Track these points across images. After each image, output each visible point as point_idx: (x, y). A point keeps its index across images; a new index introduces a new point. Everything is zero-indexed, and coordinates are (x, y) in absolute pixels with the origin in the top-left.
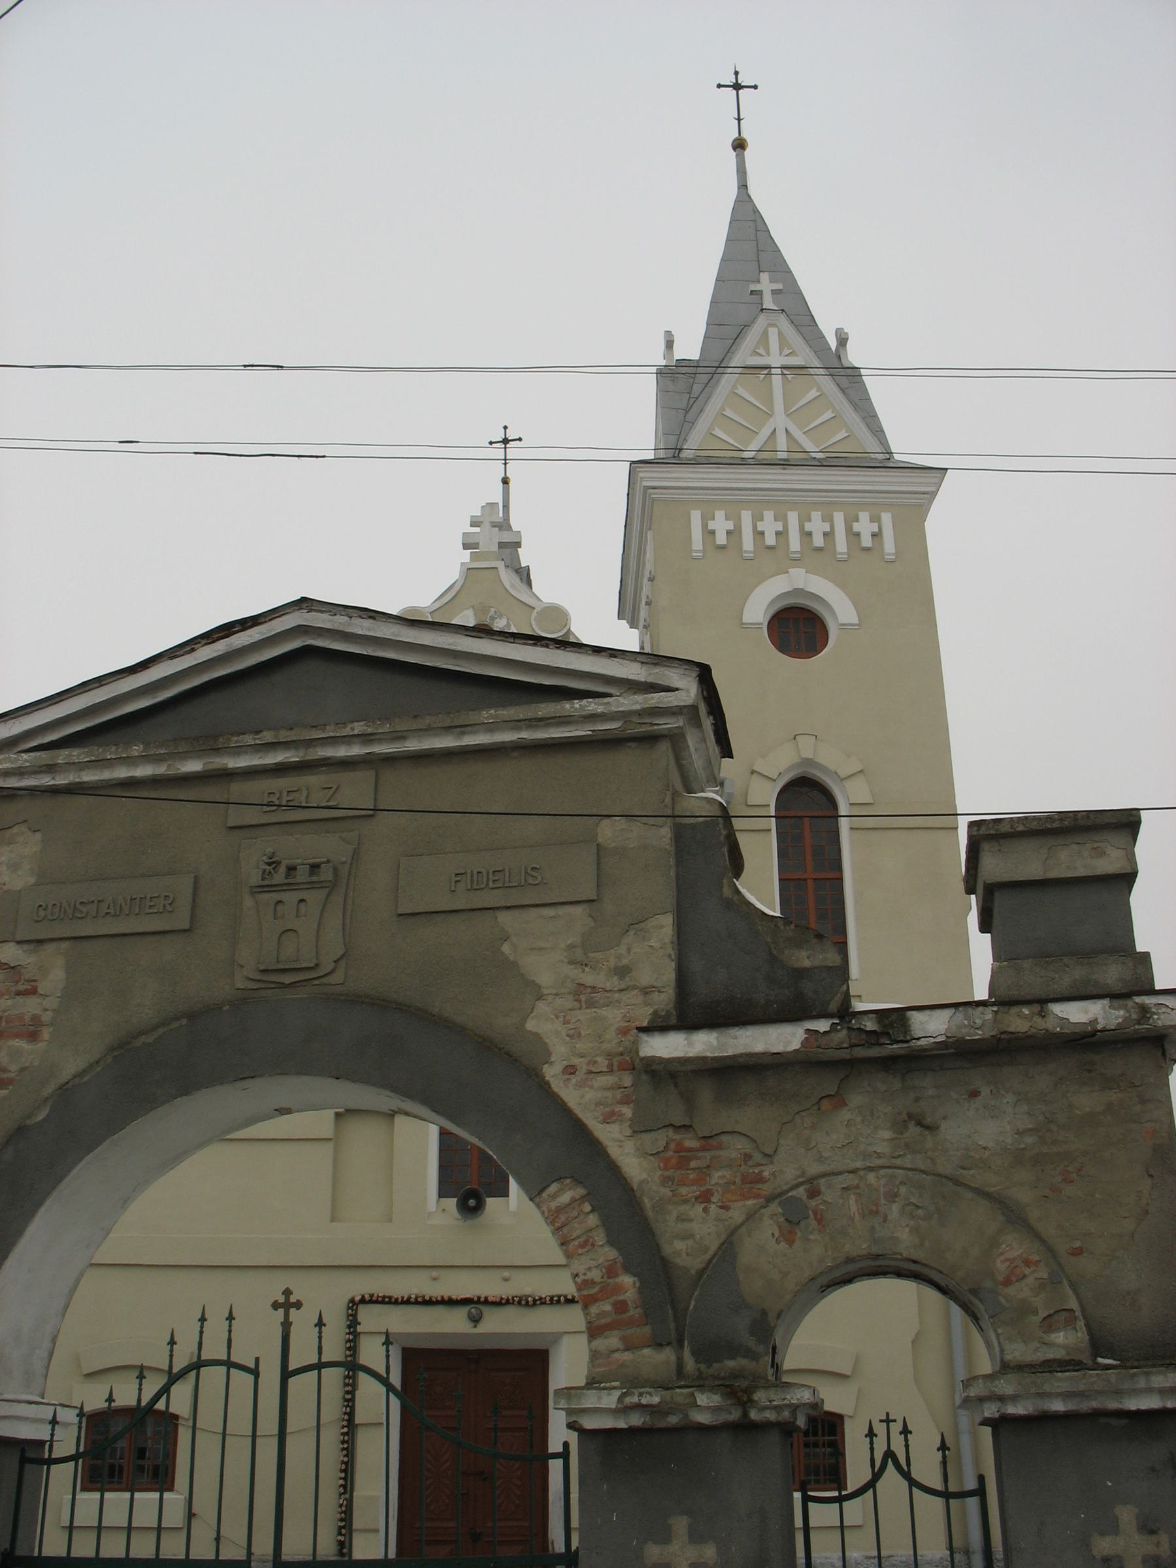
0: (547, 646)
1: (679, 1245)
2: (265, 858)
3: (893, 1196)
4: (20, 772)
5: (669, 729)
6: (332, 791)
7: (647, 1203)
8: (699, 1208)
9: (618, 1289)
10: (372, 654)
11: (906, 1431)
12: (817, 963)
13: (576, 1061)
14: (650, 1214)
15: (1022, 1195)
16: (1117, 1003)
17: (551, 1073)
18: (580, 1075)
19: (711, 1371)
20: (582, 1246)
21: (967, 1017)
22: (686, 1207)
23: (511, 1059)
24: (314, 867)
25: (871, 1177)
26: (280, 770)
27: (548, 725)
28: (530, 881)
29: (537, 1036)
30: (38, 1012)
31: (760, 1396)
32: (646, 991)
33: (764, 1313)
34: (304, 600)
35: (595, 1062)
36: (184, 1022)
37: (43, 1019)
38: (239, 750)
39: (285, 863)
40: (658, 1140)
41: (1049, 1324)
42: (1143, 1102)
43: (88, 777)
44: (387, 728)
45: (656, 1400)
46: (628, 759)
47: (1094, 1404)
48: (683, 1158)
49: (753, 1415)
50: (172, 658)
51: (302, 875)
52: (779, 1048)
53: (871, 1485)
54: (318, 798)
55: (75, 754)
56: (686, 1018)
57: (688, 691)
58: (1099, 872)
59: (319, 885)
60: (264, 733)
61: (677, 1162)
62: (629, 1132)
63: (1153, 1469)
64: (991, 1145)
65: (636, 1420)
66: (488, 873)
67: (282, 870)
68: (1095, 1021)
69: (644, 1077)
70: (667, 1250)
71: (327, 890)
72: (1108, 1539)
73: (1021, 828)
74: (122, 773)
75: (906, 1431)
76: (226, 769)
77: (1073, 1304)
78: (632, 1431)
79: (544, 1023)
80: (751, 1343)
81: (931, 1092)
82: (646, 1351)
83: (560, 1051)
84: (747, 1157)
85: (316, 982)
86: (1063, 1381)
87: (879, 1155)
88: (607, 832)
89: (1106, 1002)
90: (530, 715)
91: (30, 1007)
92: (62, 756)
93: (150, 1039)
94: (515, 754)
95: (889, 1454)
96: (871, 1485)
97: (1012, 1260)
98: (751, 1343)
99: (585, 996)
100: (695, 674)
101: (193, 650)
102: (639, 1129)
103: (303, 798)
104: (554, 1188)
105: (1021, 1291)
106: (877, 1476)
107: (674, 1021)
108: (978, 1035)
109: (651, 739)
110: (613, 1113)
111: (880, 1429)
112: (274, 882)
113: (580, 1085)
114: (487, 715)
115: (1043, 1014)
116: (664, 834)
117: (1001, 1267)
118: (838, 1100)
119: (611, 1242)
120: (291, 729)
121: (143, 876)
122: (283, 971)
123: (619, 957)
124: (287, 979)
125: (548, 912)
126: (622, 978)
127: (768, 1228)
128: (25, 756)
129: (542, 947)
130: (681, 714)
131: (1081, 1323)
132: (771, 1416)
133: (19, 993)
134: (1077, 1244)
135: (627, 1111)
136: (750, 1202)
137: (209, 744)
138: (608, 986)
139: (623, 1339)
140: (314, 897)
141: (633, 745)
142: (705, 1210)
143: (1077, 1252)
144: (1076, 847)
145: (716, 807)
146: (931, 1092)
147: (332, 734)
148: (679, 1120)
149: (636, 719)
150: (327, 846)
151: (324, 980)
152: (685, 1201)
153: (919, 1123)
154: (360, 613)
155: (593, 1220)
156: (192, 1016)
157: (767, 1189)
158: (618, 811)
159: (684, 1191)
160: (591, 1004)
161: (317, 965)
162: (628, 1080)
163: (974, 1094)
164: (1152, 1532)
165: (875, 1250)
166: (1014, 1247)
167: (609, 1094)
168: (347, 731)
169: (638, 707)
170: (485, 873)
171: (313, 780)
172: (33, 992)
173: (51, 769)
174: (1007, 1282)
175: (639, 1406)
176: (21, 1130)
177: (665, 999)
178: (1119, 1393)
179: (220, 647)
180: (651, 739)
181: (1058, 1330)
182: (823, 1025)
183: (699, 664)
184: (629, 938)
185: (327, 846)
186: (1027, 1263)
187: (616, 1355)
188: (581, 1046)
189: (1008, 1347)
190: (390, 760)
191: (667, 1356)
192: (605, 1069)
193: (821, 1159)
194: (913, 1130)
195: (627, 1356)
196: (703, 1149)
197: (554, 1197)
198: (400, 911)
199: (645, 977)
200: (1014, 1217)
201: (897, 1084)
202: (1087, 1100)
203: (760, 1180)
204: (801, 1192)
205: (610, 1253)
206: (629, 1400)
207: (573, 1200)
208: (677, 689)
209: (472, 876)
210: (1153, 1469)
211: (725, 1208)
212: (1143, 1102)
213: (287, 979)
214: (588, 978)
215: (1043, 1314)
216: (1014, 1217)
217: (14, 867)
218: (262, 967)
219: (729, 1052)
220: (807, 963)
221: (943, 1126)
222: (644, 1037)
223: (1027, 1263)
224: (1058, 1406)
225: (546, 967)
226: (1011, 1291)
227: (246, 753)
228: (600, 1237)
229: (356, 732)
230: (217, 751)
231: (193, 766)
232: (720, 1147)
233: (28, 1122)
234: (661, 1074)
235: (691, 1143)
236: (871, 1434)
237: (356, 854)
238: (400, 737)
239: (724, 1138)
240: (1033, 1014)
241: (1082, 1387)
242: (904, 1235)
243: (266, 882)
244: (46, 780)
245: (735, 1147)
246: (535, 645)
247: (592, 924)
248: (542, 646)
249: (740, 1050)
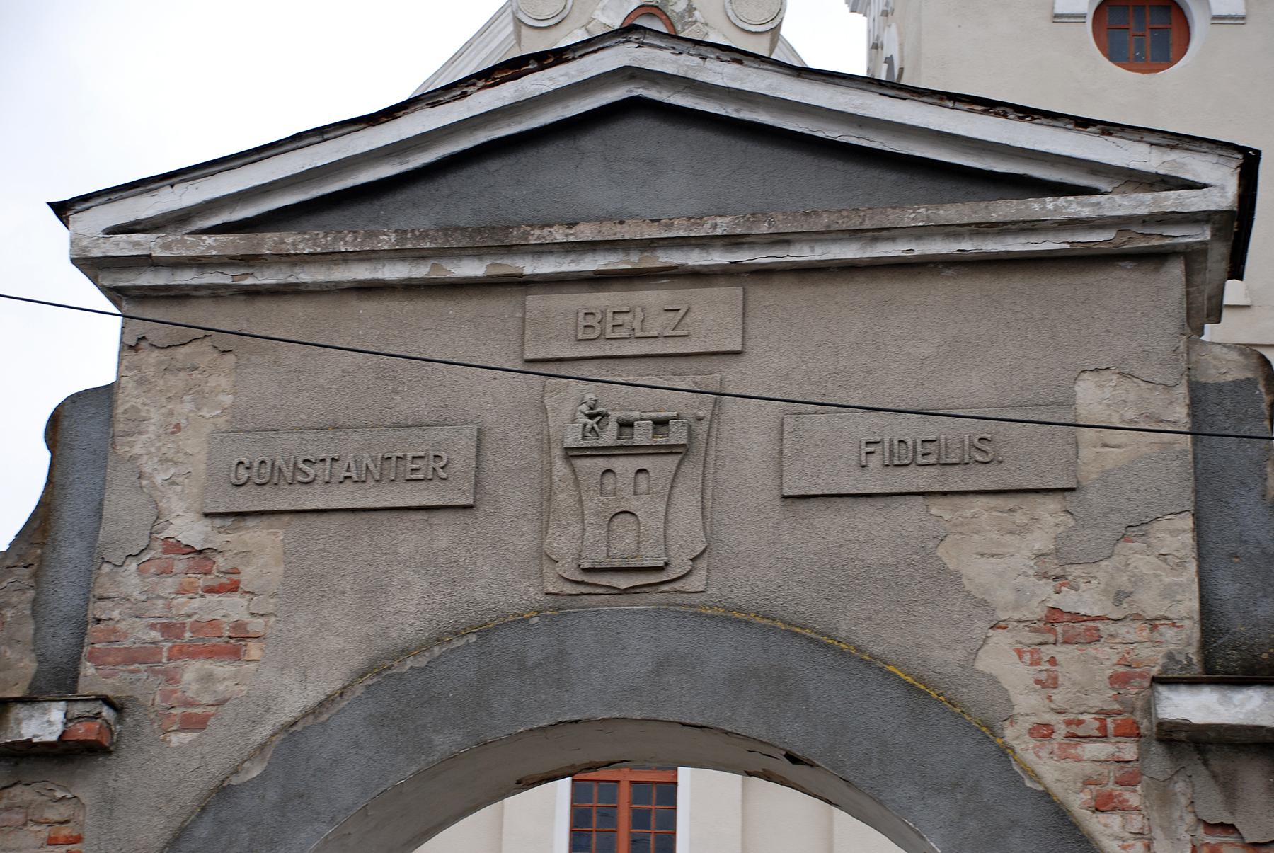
0: (1005, 116)
2: (584, 408)
4: (199, 263)
5: (1187, 245)
6: (682, 313)
10: (734, 115)
24: (661, 423)
28: (979, 458)
30: (245, 618)
35: (1080, 722)
36: (473, 638)
37: (250, 628)
39: (614, 416)
50: (433, 105)
51: (642, 435)
57: (1223, 188)
59: (669, 450)
60: (582, 227)
66: (915, 443)
67: (613, 426)
69: (1156, 749)
71: (679, 457)
76: (520, 276)
79: (1003, 663)
85: (665, 588)
91: (232, 608)
92: (268, 242)
93: (422, 661)
94: (949, 272)
100: (1235, 164)
101: (465, 95)
103: (637, 324)
107: (1197, 671)
109: (1156, 257)
112: (602, 443)
120: (621, 223)
121: (400, 425)
128: (209, 240)
130: (1207, 222)
133: (210, 590)
140: (661, 466)
141: (1129, 265)
147: (682, 233)
151: (677, 586)
154: (719, 53)
156: (484, 631)
161: (666, 564)
162: (1129, 751)
170: (910, 444)
171: (652, 298)
172: (234, 588)
176: (223, 791)
177: (1182, 639)
183: (1243, 150)
188: (1059, 697)
192: (1097, 733)
198: (786, 492)
208: (1205, 186)
209: (891, 445)
213: (623, 582)
214: (1068, 601)
218: (586, 565)
227: (551, 253)
229: (719, 232)
230: (509, 249)
233: (235, 780)
234: (1187, 742)
243: (588, 443)
246: (986, 112)
247: (1072, 523)
248: (997, 114)
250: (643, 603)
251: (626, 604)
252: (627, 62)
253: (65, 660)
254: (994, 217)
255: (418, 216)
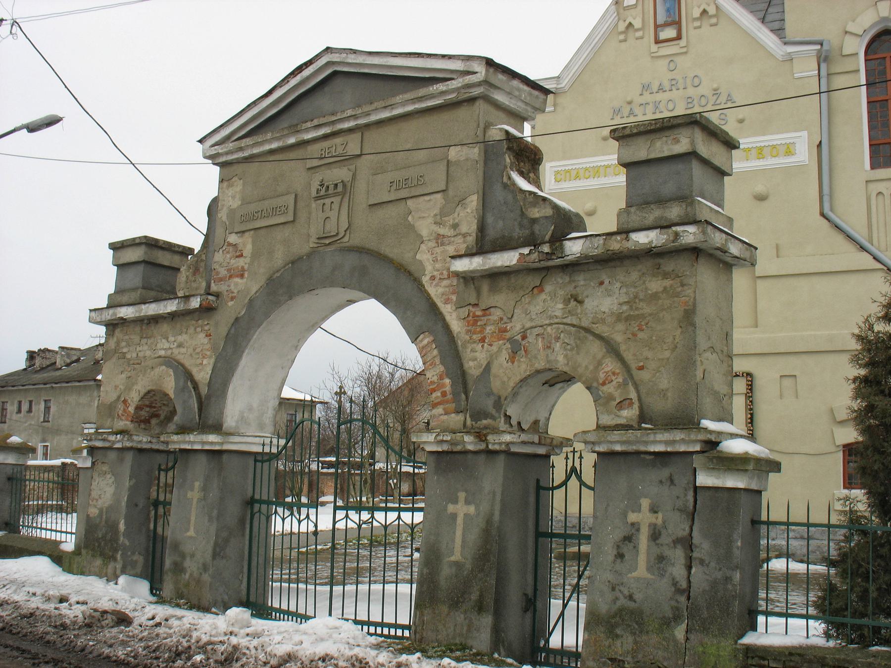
1: (471, 364)
3: (557, 339)
7: (460, 343)
8: (480, 345)
9: (443, 385)
11: (581, 457)
12: (542, 215)
13: (435, 273)
14: (460, 348)
15: (619, 338)
16: (664, 231)
17: (425, 280)
18: (437, 280)
19: (477, 425)
20: (431, 365)
21: (591, 243)
22: (475, 345)
23: (410, 273)
25: (549, 329)
26: (326, 137)
27: (427, 99)
29: (420, 261)
31: (490, 438)
32: (465, 236)
33: (500, 397)
34: (328, 48)
38: (307, 130)
40: (464, 312)
41: (620, 406)
42: (682, 285)
43: (256, 151)
44: (360, 111)
45: (449, 438)
46: (463, 113)
47: (635, 448)
48: (476, 319)
49: (490, 447)
52: (507, 264)
53: (564, 483)
54: (340, 150)
55: (248, 141)
56: (482, 247)
58: (674, 153)
61: (472, 321)
62: (454, 308)
63: (661, 482)
64: (607, 311)
65: (445, 447)
68: (651, 242)
69: (461, 280)
70: (466, 366)
72: (635, 514)
73: (635, 131)
74: (267, 147)
75: (581, 457)
77: (633, 395)
78: (443, 452)
79: (424, 256)
80: (493, 412)
81: (582, 283)
82: (453, 415)
83: (429, 268)
84: (501, 319)
86: (616, 436)
87: (557, 317)
88: (453, 153)
89: (658, 231)
90: (416, 96)
91: (241, 262)
92: (244, 143)
95: (574, 469)
96: (564, 483)
97: (607, 373)
98: (493, 412)
99: (440, 240)
102: (459, 307)
104: (421, 337)
105: (609, 389)
106: (568, 478)
108: (596, 252)
109: (472, 100)
110: (448, 299)
111: (570, 456)
113: (437, 285)
114: (398, 99)
115: (627, 239)
116: (475, 152)
117: (602, 376)
118: (540, 288)
119: (442, 363)
122: (326, 237)
123: (454, 219)
124: (327, 241)
125: (427, 198)
126: (455, 230)
127: (505, 355)
129: (424, 217)
131: (636, 406)
132: (497, 447)
134: (641, 364)
135: (454, 298)
136: (501, 342)
137: (295, 129)
138: (449, 234)
139: (444, 409)
142: (483, 346)
143: (641, 368)
144: (664, 139)
145: (503, 133)
146: (582, 283)
148: (473, 301)
149: (463, 91)
150: (341, 174)
152: (475, 342)
153: (576, 300)
155: (435, 352)
157: (508, 335)
158: (457, 142)
159: (474, 337)
160: (443, 244)
163: (602, 283)
164: (656, 512)
165: (547, 366)
166: (610, 365)
167: (447, 289)
168: (345, 115)
169: (460, 85)
171: (338, 140)
173: (241, 149)
174: (604, 384)
175: (442, 441)
176: (237, 319)
178: (646, 443)
179: (298, 78)
180: (472, 100)
181: (624, 409)
182: (526, 251)
184: (458, 209)
185: (341, 174)
186: (614, 374)
187: (442, 417)
188: (438, 266)
189: (600, 417)
190: (367, 126)
191: (460, 417)
193: (531, 320)
194: (573, 303)
195: (446, 417)
196: (484, 315)
197: (421, 341)
199: (464, 229)
200: (613, 350)
201: (567, 279)
202: (655, 285)
203: (505, 331)
204: (519, 337)
205: (441, 368)
206: (440, 438)
207: (429, 343)
210: (661, 482)
211: (491, 345)
212: (682, 285)
213: (327, 241)
215: (618, 400)
216: (613, 350)
217: (233, 197)
219: (487, 267)
220: (537, 215)
221: (586, 301)
222: (453, 261)
223: (614, 374)
224: (618, 448)
225: (425, 227)
226: (605, 388)
228: (438, 361)
231: (292, 140)
232: (490, 315)
235: (479, 313)
236: (567, 458)
237: (354, 175)
238: (368, 114)
239: (492, 310)
240: (622, 240)
241: (624, 439)
242: (561, 358)
244: (240, 155)
245: (496, 314)
249: (491, 265)
250: (332, 248)
251: (329, 249)
252: (328, 60)
253: (699, 374)
254: (420, 95)
255: (285, 122)
